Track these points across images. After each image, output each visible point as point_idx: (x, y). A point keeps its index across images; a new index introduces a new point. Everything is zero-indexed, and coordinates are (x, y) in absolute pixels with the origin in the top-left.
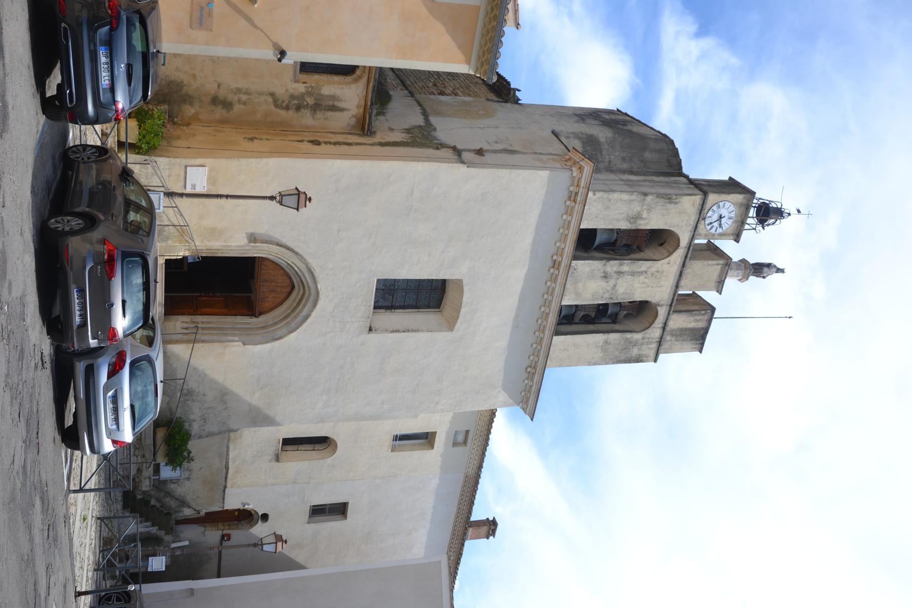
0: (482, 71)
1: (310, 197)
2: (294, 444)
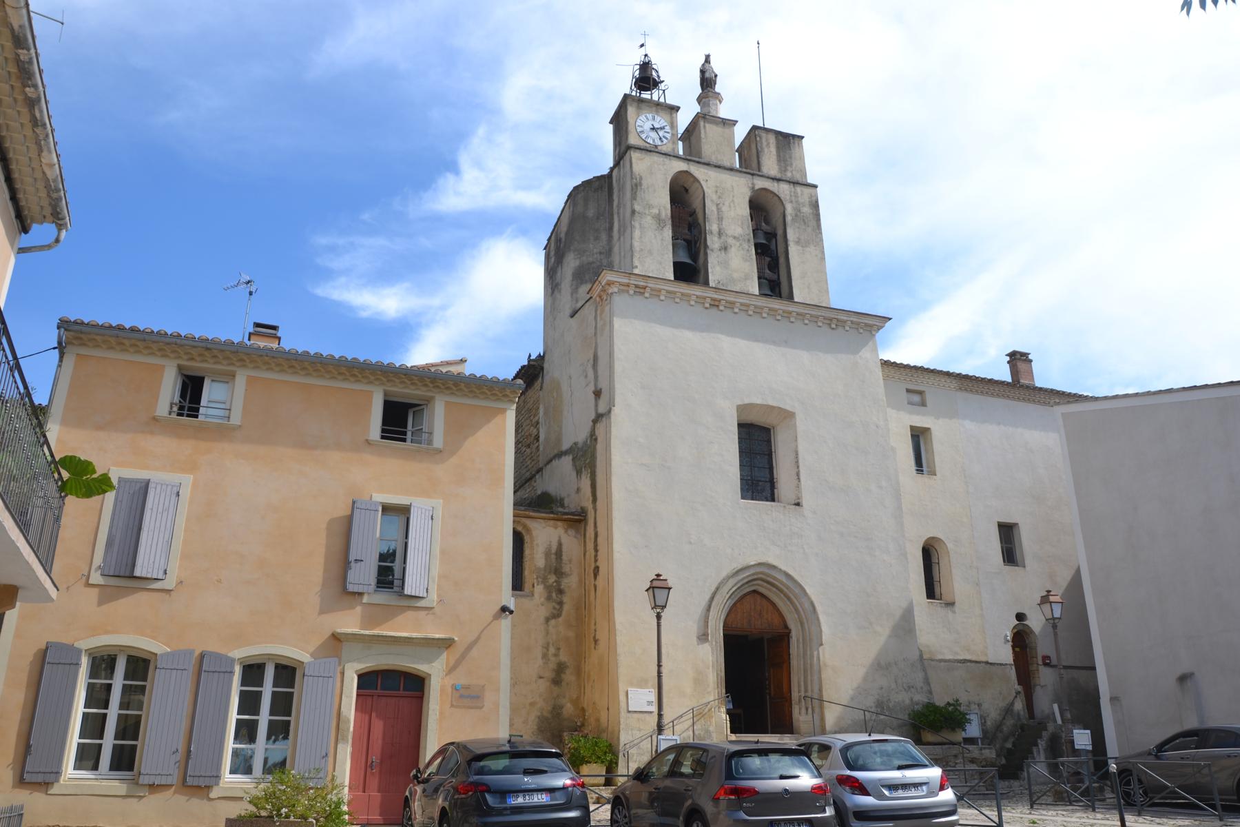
1: (656, 575)
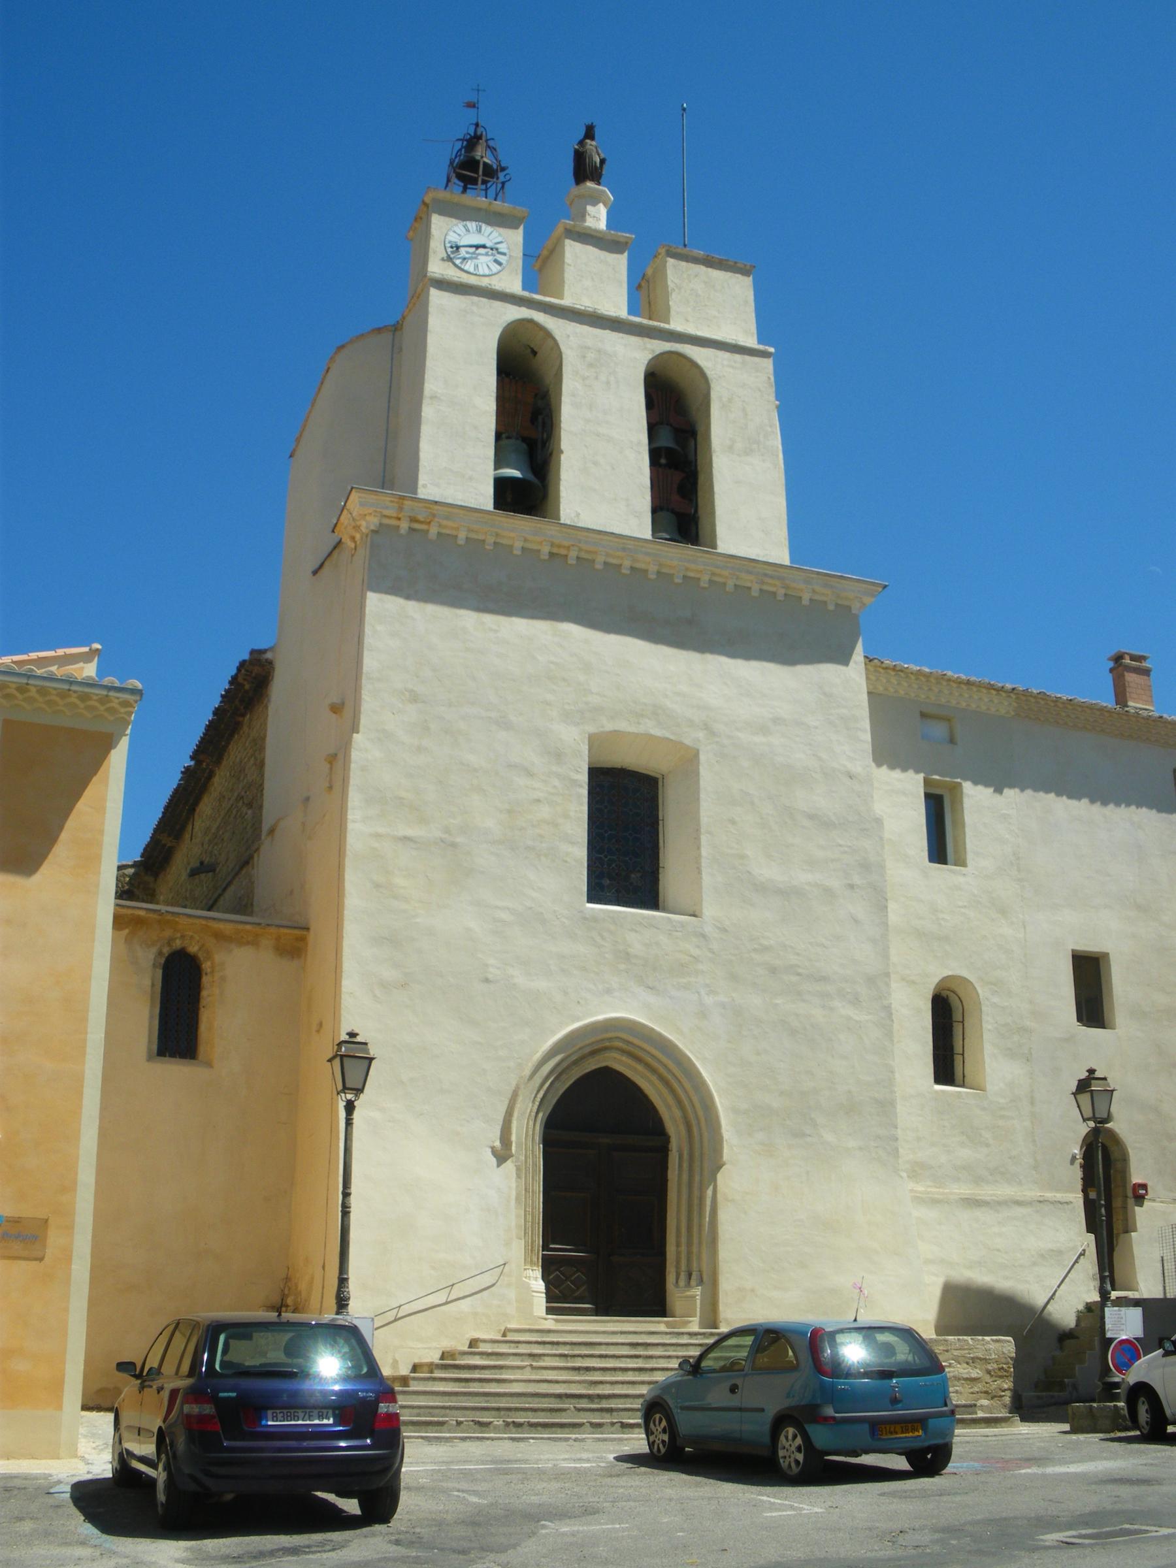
0: (123, 710)
1: (348, 1034)
2: (952, 1061)
